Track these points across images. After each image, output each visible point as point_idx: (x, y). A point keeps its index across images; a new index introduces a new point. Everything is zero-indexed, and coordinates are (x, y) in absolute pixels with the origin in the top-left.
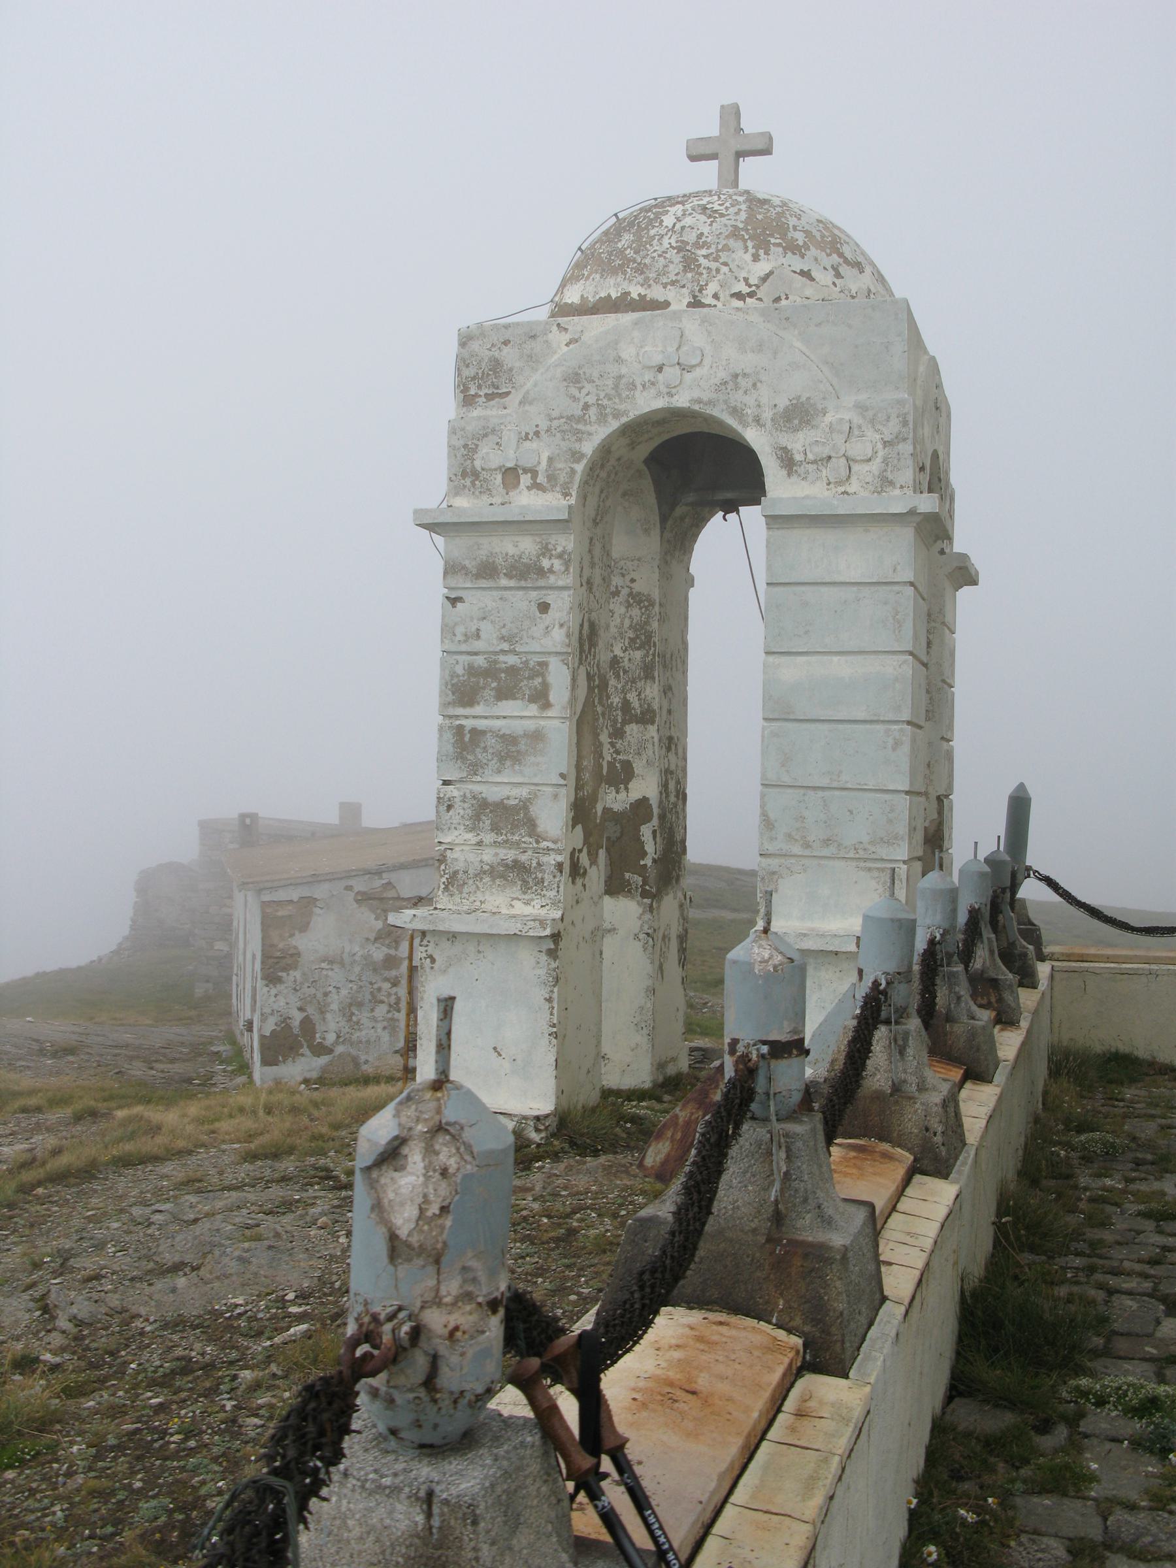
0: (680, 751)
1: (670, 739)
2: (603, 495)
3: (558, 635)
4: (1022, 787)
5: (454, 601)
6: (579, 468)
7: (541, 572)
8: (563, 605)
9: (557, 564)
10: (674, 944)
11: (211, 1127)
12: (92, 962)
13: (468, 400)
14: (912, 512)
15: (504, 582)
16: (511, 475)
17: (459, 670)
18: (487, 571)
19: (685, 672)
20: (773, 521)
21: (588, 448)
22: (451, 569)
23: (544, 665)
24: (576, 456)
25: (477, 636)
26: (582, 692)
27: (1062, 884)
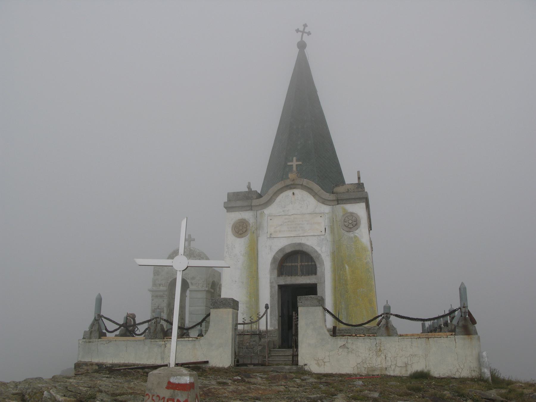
0: (184, 320)
1: (182, 318)
2: (354, 380)
3: (165, 304)
4: (99, 295)
5: (153, 300)
6: (168, 284)
7: (163, 297)
8: (166, 301)
9: (165, 296)
10: (75, 377)
11: (115, 398)
12: (40, 379)
13: (155, 275)
14: (205, 290)
15: (159, 298)
16: (160, 285)
17: (153, 308)
18: (157, 296)
19: (185, 309)
20: (190, 291)
21: (169, 282)
22: (152, 296)
23: (163, 308)
24: (168, 283)
25: (156, 304)
26: (168, 311)
27: (400, 315)
